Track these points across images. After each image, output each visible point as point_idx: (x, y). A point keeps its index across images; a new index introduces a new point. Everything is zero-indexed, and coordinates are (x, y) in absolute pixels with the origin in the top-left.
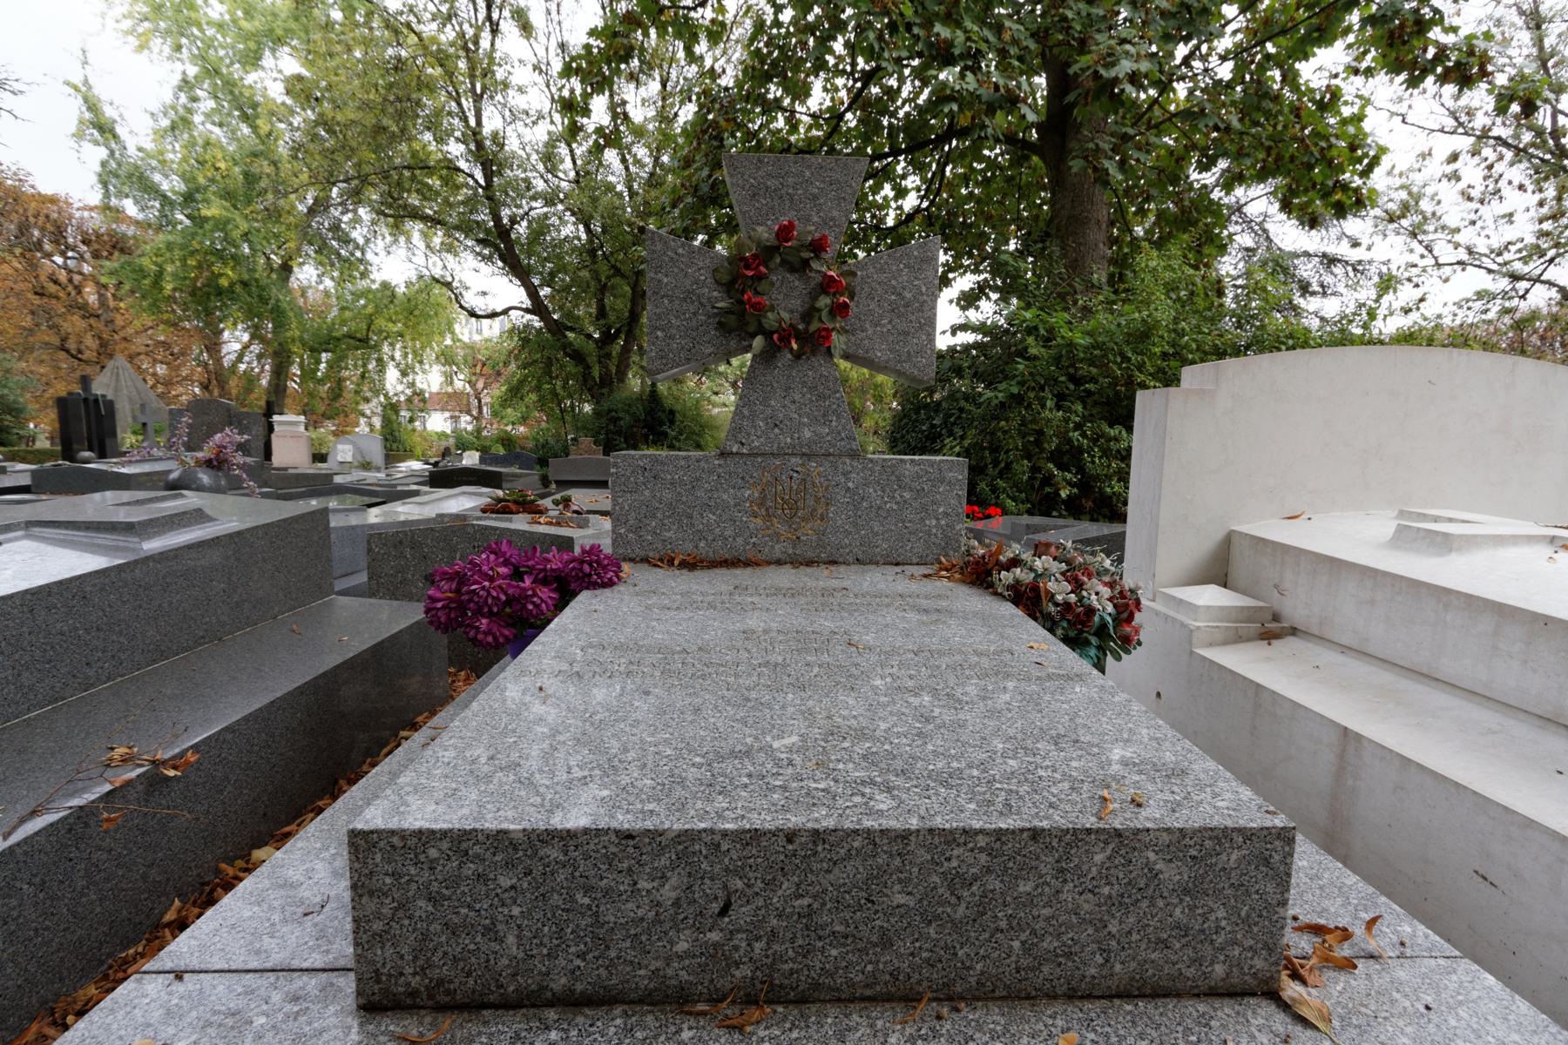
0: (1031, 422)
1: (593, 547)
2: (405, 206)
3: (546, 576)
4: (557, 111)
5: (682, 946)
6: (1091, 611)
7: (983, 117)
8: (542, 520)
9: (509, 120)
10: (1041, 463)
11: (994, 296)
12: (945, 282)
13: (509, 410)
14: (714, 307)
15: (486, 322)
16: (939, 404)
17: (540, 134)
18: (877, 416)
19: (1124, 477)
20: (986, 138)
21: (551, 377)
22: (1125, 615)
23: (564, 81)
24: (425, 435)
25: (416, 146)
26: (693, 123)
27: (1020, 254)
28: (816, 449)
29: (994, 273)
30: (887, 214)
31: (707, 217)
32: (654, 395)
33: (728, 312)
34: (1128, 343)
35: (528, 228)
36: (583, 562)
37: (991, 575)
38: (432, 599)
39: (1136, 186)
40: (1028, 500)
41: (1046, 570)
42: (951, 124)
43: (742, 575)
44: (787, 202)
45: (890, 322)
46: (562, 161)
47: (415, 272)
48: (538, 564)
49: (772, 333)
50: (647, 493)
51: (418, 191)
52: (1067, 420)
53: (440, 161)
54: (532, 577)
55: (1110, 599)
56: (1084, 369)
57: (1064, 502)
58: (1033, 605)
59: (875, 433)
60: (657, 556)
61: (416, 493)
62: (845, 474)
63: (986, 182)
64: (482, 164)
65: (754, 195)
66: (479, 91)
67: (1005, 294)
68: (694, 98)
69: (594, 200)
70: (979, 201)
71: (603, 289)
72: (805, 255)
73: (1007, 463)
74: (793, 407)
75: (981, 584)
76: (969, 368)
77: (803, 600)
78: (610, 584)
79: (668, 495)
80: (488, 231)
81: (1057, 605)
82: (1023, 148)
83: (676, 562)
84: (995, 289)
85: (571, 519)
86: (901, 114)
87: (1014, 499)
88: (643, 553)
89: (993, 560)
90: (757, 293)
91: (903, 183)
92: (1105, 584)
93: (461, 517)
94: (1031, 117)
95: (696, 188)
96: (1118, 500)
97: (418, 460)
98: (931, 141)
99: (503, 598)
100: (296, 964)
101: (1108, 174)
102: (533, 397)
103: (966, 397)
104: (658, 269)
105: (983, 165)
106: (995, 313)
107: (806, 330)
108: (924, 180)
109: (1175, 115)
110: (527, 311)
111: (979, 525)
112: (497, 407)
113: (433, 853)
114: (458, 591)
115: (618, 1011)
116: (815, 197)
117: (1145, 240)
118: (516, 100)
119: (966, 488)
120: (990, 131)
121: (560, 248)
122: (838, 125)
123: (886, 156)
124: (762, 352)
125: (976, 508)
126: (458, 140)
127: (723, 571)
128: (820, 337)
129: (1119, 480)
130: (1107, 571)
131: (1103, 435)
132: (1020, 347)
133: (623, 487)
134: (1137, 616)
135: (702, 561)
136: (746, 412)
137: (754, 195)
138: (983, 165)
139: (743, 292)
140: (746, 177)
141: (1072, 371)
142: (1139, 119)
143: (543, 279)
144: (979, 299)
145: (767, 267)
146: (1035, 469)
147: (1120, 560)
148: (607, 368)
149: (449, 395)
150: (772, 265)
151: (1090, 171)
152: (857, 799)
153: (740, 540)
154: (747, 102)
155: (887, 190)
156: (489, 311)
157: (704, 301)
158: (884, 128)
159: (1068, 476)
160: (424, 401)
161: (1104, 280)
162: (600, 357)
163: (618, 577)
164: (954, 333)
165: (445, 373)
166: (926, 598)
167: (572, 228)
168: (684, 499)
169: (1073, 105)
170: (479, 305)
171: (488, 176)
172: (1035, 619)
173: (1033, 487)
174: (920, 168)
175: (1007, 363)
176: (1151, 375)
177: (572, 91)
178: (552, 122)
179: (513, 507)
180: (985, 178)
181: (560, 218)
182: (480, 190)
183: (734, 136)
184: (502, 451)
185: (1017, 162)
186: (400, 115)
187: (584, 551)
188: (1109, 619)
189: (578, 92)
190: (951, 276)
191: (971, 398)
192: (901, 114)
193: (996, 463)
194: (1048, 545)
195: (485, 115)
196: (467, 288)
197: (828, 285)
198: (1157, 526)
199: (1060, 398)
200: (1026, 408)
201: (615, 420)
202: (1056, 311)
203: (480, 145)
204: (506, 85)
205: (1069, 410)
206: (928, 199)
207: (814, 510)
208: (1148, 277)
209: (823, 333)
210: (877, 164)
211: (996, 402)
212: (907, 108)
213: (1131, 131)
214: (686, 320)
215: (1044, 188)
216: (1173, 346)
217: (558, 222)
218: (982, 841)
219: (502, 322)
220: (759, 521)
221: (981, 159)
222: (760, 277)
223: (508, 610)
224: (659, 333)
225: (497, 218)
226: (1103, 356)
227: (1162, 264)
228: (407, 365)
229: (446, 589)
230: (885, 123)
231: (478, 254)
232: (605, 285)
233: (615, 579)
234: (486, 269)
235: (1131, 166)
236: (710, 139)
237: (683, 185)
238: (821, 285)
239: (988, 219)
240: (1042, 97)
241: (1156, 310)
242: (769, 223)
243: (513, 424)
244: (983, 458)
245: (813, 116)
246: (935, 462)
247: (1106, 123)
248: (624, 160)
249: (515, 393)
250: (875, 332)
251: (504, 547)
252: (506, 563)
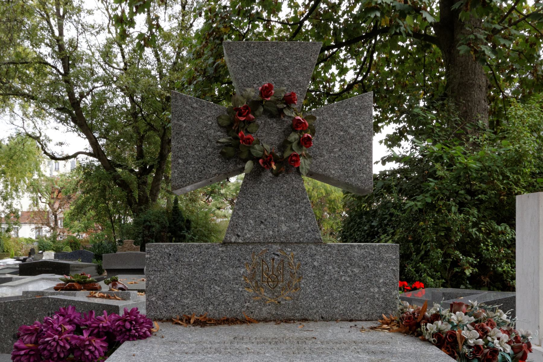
0: (442, 222)
1: (132, 310)
2: (10, 88)
3: (99, 332)
4: (113, 25)
6: (495, 352)
7: (398, 20)
8: (97, 295)
9: (81, 31)
10: (450, 251)
11: (410, 137)
12: (377, 129)
13: (76, 223)
14: (218, 142)
15: (62, 163)
16: (375, 211)
17: (102, 39)
18: (331, 222)
19: (511, 260)
20: (400, 33)
21: (105, 199)
22: (520, 355)
23: (117, 5)
24: (17, 241)
25: (20, 49)
26: (202, 30)
27: (428, 108)
28: (291, 238)
29: (410, 122)
30: (334, 86)
31: (212, 90)
32: (176, 210)
33: (227, 145)
34: (506, 166)
35: (92, 100)
36: (125, 321)
37: (420, 327)
38: (18, 349)
39: (504, 62)
40: (442, 278)
41: (460, 322)
42: (375, 26)
43: (239, 329)
45: (340, 150)
46: (116, 57)
47: (14, 131)
48: (93, 323)
49: (258, 159)
50: (171, 272)
51: (19, 78)
52: (467, 221)
53: (35, 58)
54: (89, 332)
55: (509, 343)
56: (477, 185)
57: (468, 278)
58: (452, 347)
59: (331, 234)
60: (178, 317)
61: (10, 280)
63: (402, 62)
64: (62, 60)
65: (245, 68)
66: (61, 14)
67: (418, 134)
68: (203, 14)
69: (136, 81)
70: (397, 75)
71: (141, 139)
72: (280, 106)
73: (426, 251)
74: (274, 210)
75: (413, 334)
76: (396, 186)
77: (284, 346)
78: (144, 336)
79: (185, 273)
80: (64, 102)
81: (469, 347)
82: (425, 40)
83: (192, 321)
84: (411, 132)
85: (117, 294)
86: (342, 20)
87: (432, 277)
88: (168, 315)
89: (421, 316)
90: (248, 132)
91: (345, 64)
92: (504, 332)
93: (41, 293)
94: (430, 19)
96: (507, 276)
97: (12, 258)
98: (362, 37)
99: (68, 347)
101: (485, 55)
102: (93, 213)
103: (395, 206)
104: (179, 118)
105: (399, 52)
106: (412, 148)
107: (282, 156)
108: (358, 63)
109: (528, 16)
110: (90, 154)
111: (409, 295)
112: (68, 220)
114: (36, 343)
116: (286, 68)
117: (512, 98)
118: (87, 19)
119: (398, 264)
120: (402, 29)
121: (113, 112)
122: (300, 28)
123: (332, 47)
124: (252, 172)
125: (406, 283)
126: (47, 45)
127: (226, 327)
128: (291, 160)
129: (507, 262)
130: (504, 322)
131: (493, 230)
132: (431, 171)
133: (154, 268)
134: (529, 355)
135: (210, 320)
136: (241, 214)
137: (245, 68)
138: (399, 52)
139: (238, 132)
141: (468, 186)
142: (503, 20)
143: (101, 133)
144: (400, 140)
145: (254, 115)
146: (446, 255)
147: (513, 315)
148: (144, 191)
149: (35, 213)
150: (257, 113)
151: (472, 53)
153: (237, 305)
154: (238, 15)
155: (334, 69)
156: (64, 156)
157: (211, 138)
158: (330, 29)
159: (471, 260)
160: (17, 217)
161: (486, 124)
162: (139, 184)
163: (150, 331)
164: (384, 163)
165: (32, 198)
166: (373, 343)
167: (122, 100)
168: (197, 275)
169: (458, 11)
170: (58, 151)
171: (66, 67)
172: (455, 358)
173: (445, 268)
174: (355, 54)
175: (422, 182)
176: (524, 188)
177: (123, 12)
178: (109, 32)
179: (77, 286)
180: (400, 60)
181: (114, 93)
182: (60, 76)
183: (230, 37)
184: (69, 250)
185: (421, 49)
186: (10, 30)
187: (126, 313)
188: (509, 358)
189: (127, 10)
190: (380, 125)
191: (398, 206)
192: (342, 20)
193: (418, 251)
194: (460, 304)
195: (65, 28)
196: (50, 141)
197: (296, 126)
199: (461, 206)
200: (437, 212)
201: (149, 228)
202: (454, 145)
203: (61, 48)
204: (79, 10)
205: (468, 213)
206: (362, 74)
207: (290, 282)
208: (517, 121)
209: (294, 158)
210: (326, 52)
211: (416, 208)
212: (346, 17)
213: (498, 27)
214: (198, 151)
215: (442, 65)
216: (539, 168)
217: (111, 96)
219: (72, 163)
220: (251, 291)
221: (397, 48)
222: (249, 122)
223: (71, 356)
224: (180, 161)
225: (71, 94)
226: (489, 176)
227: (526, 112)
228: (7, 193)
229: (27, 342)
230: (332, 26)
231: (58, 118)
232: (143, 136)
233: (148, 333)
234: (62, 127)
235: (500, 49)
236: (214, 39)
237: (196, 70)
238: (291, 126)
239: (404, 86)
240: (437, 8)
241: (525, 143)
242: (255, 86)
243: (79, 231)
244: (408, 248)
245: (282, 23)
246: (375, 247)
247: (481, 22)
248: (157, 55)
249: (80, 210)
250: (330, 157)
251: (70, 312)
252: (70, 322)
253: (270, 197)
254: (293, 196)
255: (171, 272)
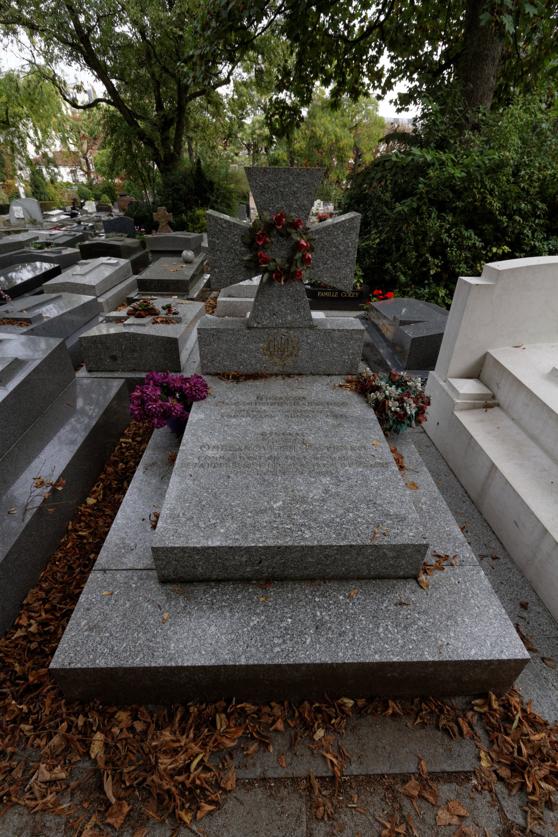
5: (248, 570)
44: (280, 196)
50: (215, 345)
62: (307, 336)
65: (262, 192)
74: (283, 305)
77: (286, 408)
78: (204, 398)
79: (225, 346)
83: (230, 377)
88: (215, 371)
95: (218, 15)
100: (136, 567)
113: (176, 552)
115: (231, 583)
116: (295, 193)
136: (260, 308)
137: (262, 192)
140: (257, 181)
146: (420, 256)
152: (300, 533)
153: (258, 365)
157: (238, 253)
159: (436, 261)
190: (393, 80)
193: (398, 250)
198: (453, 349)
201: (177, 191)
205: (444, 220)
218: (335, 548)
220: (267, 357)
224: (216, 270)
242: (270, 208)
253: (280, 297)
254: (296, 296)
255: (215, 345)
